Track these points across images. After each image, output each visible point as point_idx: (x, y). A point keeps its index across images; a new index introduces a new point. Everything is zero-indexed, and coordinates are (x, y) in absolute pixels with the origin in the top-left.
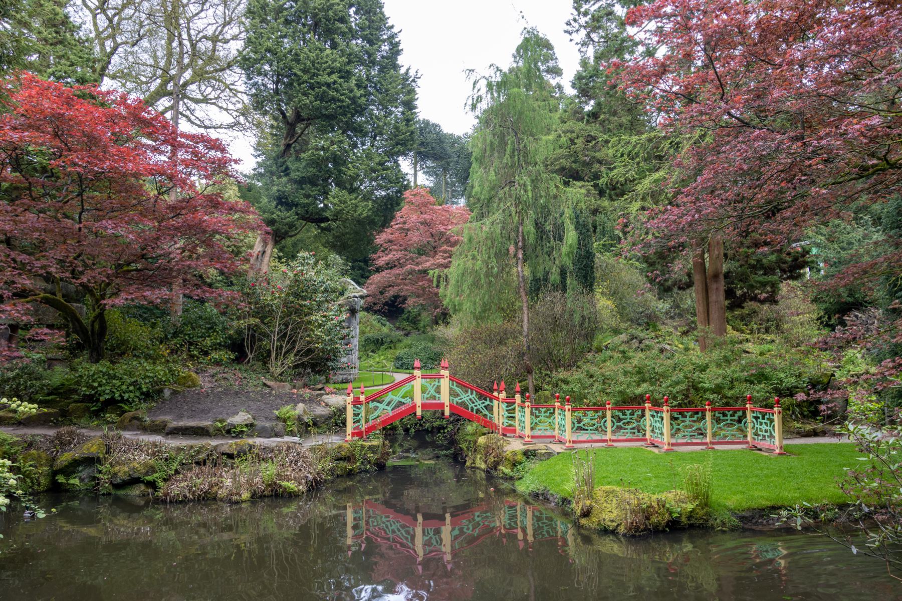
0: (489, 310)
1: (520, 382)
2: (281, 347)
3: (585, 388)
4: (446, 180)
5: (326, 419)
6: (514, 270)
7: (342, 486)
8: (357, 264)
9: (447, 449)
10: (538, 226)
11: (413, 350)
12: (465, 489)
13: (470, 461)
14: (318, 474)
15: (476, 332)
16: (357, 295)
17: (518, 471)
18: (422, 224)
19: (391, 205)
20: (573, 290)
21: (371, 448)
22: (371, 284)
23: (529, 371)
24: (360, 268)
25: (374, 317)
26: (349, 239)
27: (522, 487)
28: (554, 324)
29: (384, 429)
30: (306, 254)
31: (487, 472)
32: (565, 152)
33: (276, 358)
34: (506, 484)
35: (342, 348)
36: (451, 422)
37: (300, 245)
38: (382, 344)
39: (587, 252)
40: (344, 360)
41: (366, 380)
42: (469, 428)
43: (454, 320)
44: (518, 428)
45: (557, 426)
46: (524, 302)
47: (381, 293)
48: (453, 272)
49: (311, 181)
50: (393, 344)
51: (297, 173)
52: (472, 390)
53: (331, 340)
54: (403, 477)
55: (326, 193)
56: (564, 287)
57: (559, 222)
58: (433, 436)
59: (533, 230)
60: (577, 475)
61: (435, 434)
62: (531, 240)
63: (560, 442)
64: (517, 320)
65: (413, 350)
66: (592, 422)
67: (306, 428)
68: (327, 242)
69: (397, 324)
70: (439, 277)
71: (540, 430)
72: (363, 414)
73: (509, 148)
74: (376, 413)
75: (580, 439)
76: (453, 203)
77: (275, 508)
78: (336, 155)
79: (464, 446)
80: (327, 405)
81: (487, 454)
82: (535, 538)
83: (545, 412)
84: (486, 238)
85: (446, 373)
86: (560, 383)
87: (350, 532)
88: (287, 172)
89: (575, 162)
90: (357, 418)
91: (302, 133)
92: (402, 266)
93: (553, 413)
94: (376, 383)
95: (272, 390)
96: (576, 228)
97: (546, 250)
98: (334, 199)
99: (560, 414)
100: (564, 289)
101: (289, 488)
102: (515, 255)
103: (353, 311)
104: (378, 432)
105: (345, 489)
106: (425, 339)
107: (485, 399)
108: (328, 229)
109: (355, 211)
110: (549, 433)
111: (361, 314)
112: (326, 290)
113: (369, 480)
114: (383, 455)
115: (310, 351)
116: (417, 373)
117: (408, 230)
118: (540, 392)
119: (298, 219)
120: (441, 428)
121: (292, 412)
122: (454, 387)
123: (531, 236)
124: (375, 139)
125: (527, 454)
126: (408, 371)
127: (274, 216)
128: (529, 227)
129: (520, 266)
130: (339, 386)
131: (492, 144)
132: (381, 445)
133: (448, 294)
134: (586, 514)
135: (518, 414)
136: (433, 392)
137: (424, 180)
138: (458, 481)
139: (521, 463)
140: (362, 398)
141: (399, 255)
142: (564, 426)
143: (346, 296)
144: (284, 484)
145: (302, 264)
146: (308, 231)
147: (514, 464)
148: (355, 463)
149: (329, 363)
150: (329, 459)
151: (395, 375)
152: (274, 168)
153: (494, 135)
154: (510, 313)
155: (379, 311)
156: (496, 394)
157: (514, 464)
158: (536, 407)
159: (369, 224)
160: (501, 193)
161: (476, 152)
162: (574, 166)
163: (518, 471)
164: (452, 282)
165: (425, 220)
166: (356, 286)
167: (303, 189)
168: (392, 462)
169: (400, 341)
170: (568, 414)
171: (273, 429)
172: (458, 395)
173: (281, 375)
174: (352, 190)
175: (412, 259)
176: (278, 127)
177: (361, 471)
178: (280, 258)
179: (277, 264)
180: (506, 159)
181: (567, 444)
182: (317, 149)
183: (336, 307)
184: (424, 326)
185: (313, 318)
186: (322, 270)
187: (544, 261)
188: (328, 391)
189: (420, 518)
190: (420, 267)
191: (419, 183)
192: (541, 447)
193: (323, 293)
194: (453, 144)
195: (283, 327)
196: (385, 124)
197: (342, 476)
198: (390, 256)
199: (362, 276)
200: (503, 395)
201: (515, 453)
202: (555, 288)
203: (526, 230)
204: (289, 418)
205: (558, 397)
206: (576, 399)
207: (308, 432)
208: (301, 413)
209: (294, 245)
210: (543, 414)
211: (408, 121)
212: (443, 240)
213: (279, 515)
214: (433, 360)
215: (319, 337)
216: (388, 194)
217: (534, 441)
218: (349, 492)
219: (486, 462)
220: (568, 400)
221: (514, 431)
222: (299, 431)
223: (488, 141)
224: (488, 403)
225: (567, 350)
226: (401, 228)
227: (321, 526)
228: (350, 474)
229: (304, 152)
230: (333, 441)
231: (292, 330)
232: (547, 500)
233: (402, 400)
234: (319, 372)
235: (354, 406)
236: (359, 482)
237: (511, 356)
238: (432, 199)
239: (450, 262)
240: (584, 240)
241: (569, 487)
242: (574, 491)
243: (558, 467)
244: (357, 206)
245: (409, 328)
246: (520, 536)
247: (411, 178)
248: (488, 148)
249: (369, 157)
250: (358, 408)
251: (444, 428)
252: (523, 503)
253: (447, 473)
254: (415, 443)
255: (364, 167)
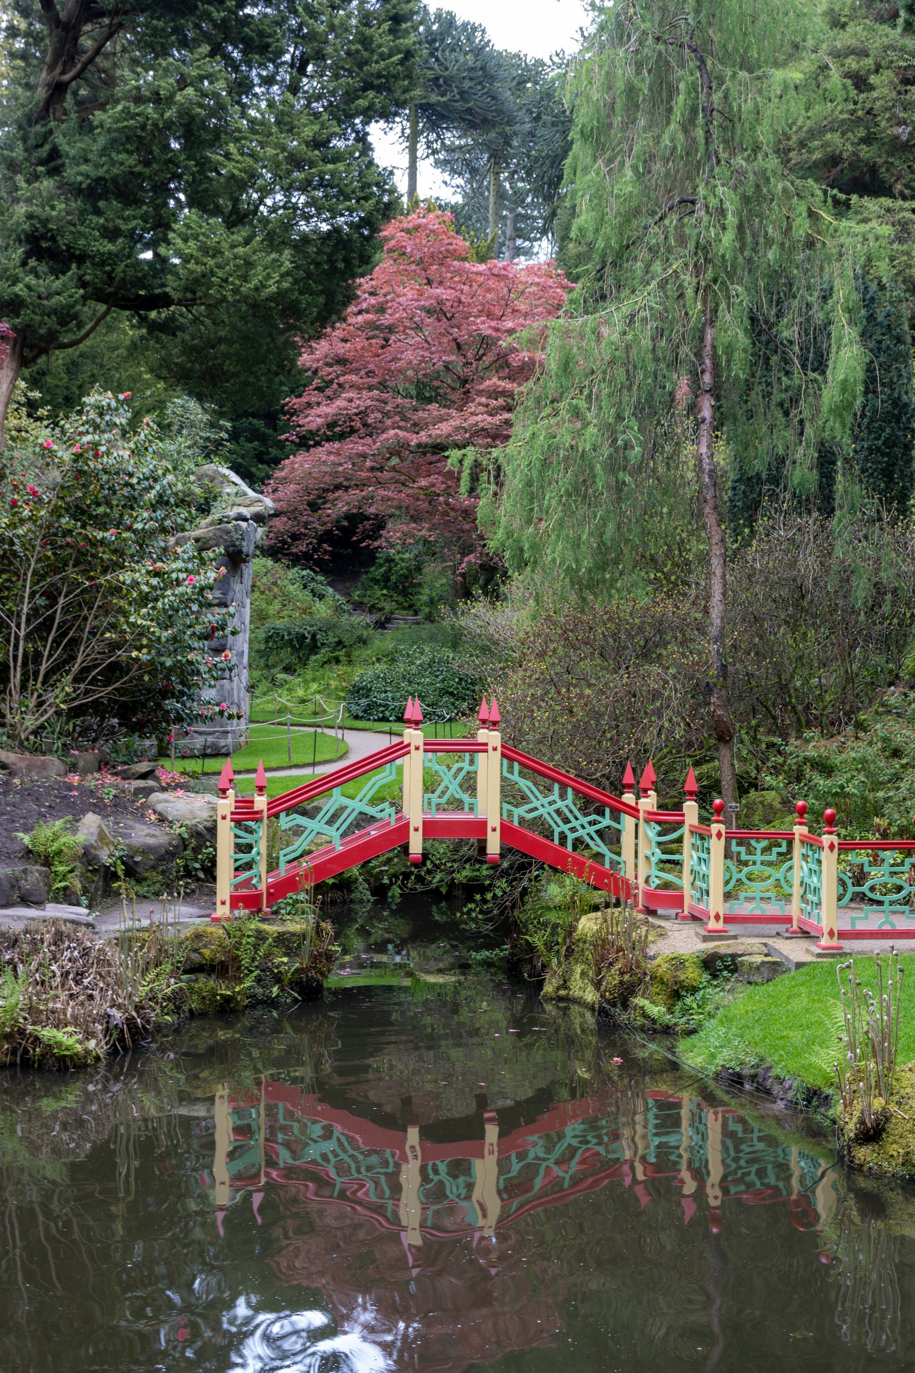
0: (616, 562)
1: (697, 764)
2: (38, 656)
3: (877, 786)
4: (499, 185)
5: (161, 859)
6: (689, 449)
7: (203, 1043)
8: (245, 422)
9: (490, 947)
10: (758, 327)
11: (401, 667)
12: (538, 1056)
13: (556, 982)
14: (138, 1008)
15: (577, 623)
16: (246, 512)
17: (686, 1011)
18: (429, 312)
19: (346, 260)
20: (852, 509)
21: (282, 940)
22: (284, 481)
23: (724, 736)
24: (255, 435)
25: (294, 573)
26: (226, 356)
27: (695, 1056)
28: (796, 605)
29: (319, 888)
30: (107, 399)
31: (602, 1012)
32: (840, 110)
33: (24, 687)
34: (652, 1046)
35: (201, 658)
36: (505, 873)
37: (88, 368)
38: (314, 648)
39: (896, 402)
40: (208, 694)
41: (269, 749)
42: (555, 891)
43: (517, 585)
44: (688, 892)
45: (797, 891)
46: (713, 539)
47: (314, 506)
48: (517, 455)
49: (124, 190)
50: (343, 650)
51: (84, 168)
52: (563, 786)
53: (174, 639)
54: (364, 1017)
55: (162, 224)
56: (826, 504)
57: (819, 317)
58: (453, 909)
59: (743, 340)
60: (849, 1026)
61: (462, 905)
62: (738, 370)
63: (805, 934)
64: (693, 592)
65: (401, 667)
66: (895, 880)
67: (105, 881)
68: (165, 363)
69: (356, 595)
70: (477, 464)
71: (749, 899)
72: (262, 847)
73: (680, 102)
74: (300, 844)
75: (861, 926)
76: (518, 252)
77: (19, 1099)
78: (192, 118)
79: (538, 940)
80: (162, 819)
81: (602, 963)
82: (725, 1191)
83: (765, 850)
84: (612, 362)
85: (492, 737)
86: (807, 768)
87: (221, 1169)
88: (53, 162)
89: (867, 140)
90: (245, 858)
91: (97, 52)
92: (371, 431)
93: (786, 856)
94: (296, 759)
95: (12, 774)
96: (865, 335)
97: (777, 396)
98: (189, 240)
99: (805, 857)
100: (828, 510)
101: (59, 1044)
102: (693, 408)
103: (235, 559)
104: (302, 896)
105: (211, 1051)
106: (432, 638)
107: (601, 813)
108: (168, 327)
109: (245, 278)
110: (772, 909)
111: (257, 565)
112: (161, 501)
113: (277, 1028)
114: (315, 958)
115: (115, 670)
116: (413, 736)
117: (391, 329)
118: (753, 793)
119: (85, 298)
120: (473, 888)
121: (67, 839)
122: (516, 777)
123: (738, 356)
124: (302, 71)
125: (713, 965)
126: (385, 726)
127: (19, 288)
128: (732, 331)
129: (704, 441)
130: (192, 765)
131: (631, 90)
132: (311, 933)
133: (501, 518)
134: (873, 1134)
135: (689, 856)
136: (454, 790)
137: (438, 185)
138: (520, 1036)
139: (694, 990)
140: (261, 802)
141: (364, 400)
142: (816, 891)
143: (215, 515)
144: (47, 1033)
145: (96, 427)
146: (110, 329)
147: (676, 993)
148: (240, 981)
149: (170, 704)
150: (167, 967)
151: (351, 738)
152: (19, 153)
153: (639, 66)
154: (673, 572)
155: (307, 556)
156: (628, 798)
157: (676, 993)
158: (741, 835)
159: (283, 314)
160: (655, 235)
161: (583, 117)
162: (866, 152)
163: (686, 1011)
164: (514, 482)
165: (440, 302)
166: (244, 487)
167: (98, 212)
168: (343, 977)
169: (363, 641)
170: (829, 859)
171: (14, 883)
172: (524, 799)
173: (35, 733)
174: (237, 218)
175: (399, 411)
176: (28, 34)
177: (256, 1002)
178: (32, 406)
179: (25, 422)
180: (672, 134)
181: (825, 941)
182: (139, 100)
183: (189, 548)
184: (432, 602)
185: (126, 577)
186: (148, 442)
187: (771, 428)
188: (165, 779)
189: (413, 1135)
190: (423, 437)
191: (422, 193)
192: (749, 946)
193: (153, 507)
194: (522, 82)
195: (41, 601)
196: (332, 28)
197: (203, 1015)
198: (340, 403)
199: (261, 458)
200: (649, 802)
201: (678, 963)
202: (802, 504)
203: (724, 339)
204: (59, 853)
205: (802, 811)
206: (850, 817)
207: (109, 893)
208: (93, 840)
209: (72, 367)
210: (758, 857)
211: (397, 19)
212: (487, 360)
213: (33, 1115)
214: (457, 698)
215: (142, 632)
216: (336, 230)
217: (733, 929)
218: (223, 1059)
219: (597, 985)
220: (831, 821)
221: (679, 901)
222: (85, 891)
223: (620, 85)
224: (606, 821)
225: (830, 678)
226: (372, 325)
227: (146, 1147)
228: (225, 1010)
229: (102, 107)
230: (180, 917)
231: (65, 610)
232: (764, 1092)
233: (371, 811)
234: (138, 729)
235: (238, 823)
236: (250, 1031)
237: (675, 693)
238: (462, 244)
239: (508, 423)
240: (888, 369)
241: (827, 1060)
242: (839, 1072)
243: (797, 1005)
244: (249, 264)
245: (388, 606)
246: (690, 1187)
247: (401, 183)
248: (618, 106)
249: (286, 123)
250: (249, 831)
251: (483, 889)
252: (697, 1099)
253: (489, 1010)
254: (403, 927)
255: (270, 151)
